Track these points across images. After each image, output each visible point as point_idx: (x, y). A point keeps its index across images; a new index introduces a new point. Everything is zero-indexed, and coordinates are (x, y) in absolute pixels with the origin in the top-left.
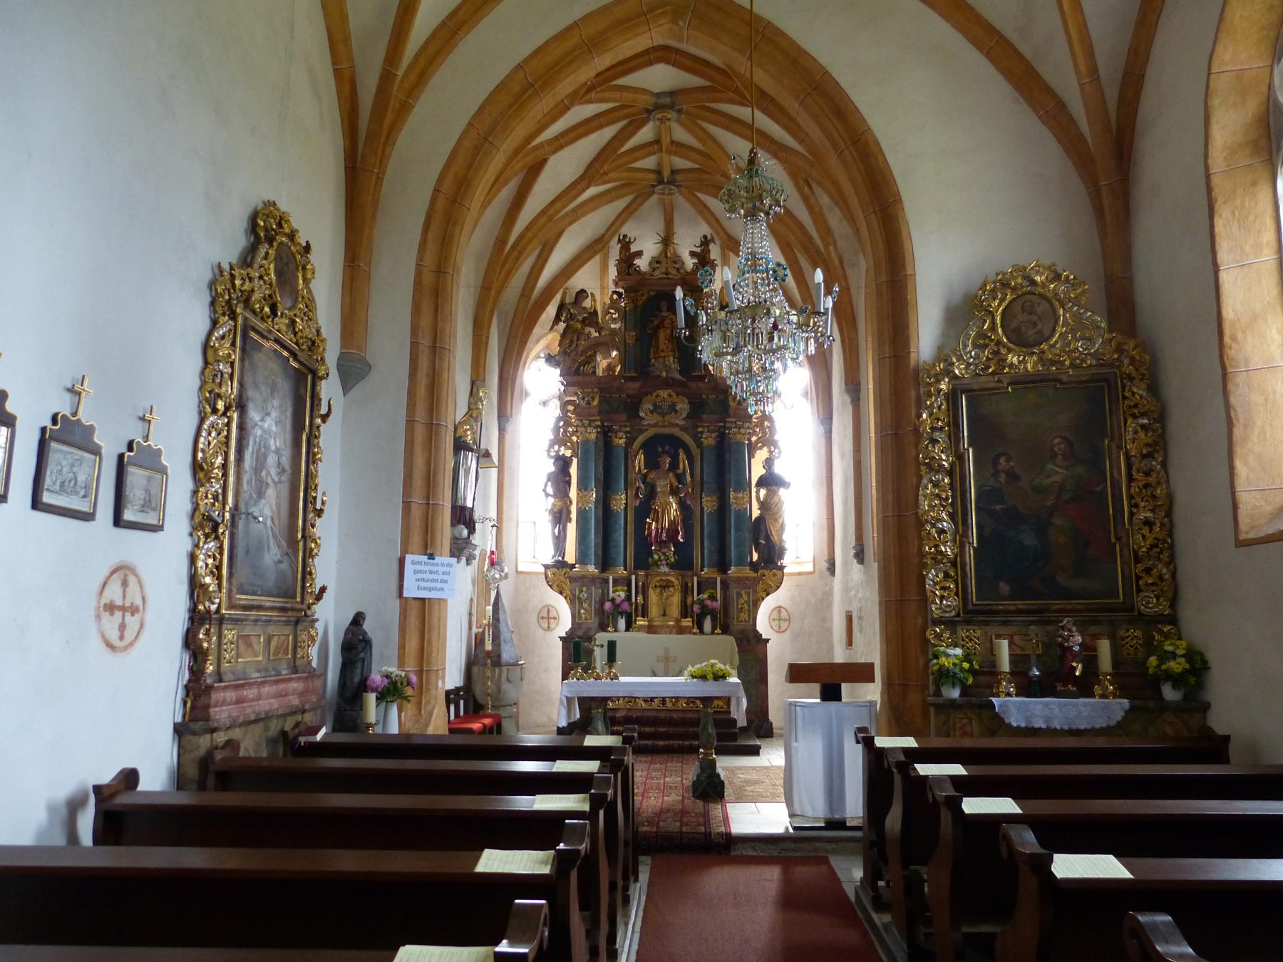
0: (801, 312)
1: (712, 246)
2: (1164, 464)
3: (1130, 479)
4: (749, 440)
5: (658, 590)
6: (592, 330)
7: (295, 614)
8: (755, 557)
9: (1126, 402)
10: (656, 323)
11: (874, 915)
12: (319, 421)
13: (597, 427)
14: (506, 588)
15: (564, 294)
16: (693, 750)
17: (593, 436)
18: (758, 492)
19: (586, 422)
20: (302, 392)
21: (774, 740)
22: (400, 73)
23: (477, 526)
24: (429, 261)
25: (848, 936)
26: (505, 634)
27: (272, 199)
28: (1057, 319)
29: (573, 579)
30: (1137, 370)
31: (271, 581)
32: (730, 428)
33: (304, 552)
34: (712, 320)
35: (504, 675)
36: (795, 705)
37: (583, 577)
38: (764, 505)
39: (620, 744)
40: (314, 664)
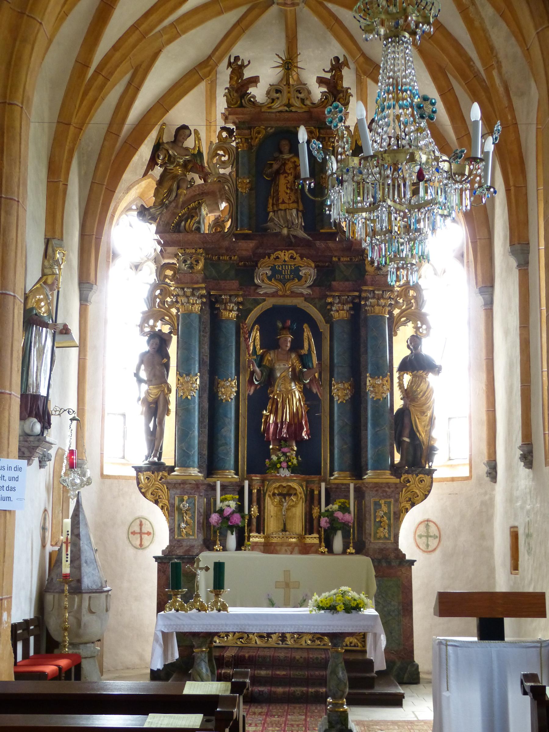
0: (454, 156)
1: (345, 72)
4: (390, 313)
6: (196, 176)
8: (397, 458)
10: (276, 167)
14: (88, 497)
15: (161, 131)
16: (320, 699)
17: (197, 308)
19: (188, 291)
21: (420, 686)
22: (206, 165)
23: (53, 418)
26: (86, 553)
29: (172, 486)
32: (366, 299)
34: (344, 168)
35: (85, 604)
36: (446, 644)
37: (184, 483)
38: (409, 395)
39: (228, 693)
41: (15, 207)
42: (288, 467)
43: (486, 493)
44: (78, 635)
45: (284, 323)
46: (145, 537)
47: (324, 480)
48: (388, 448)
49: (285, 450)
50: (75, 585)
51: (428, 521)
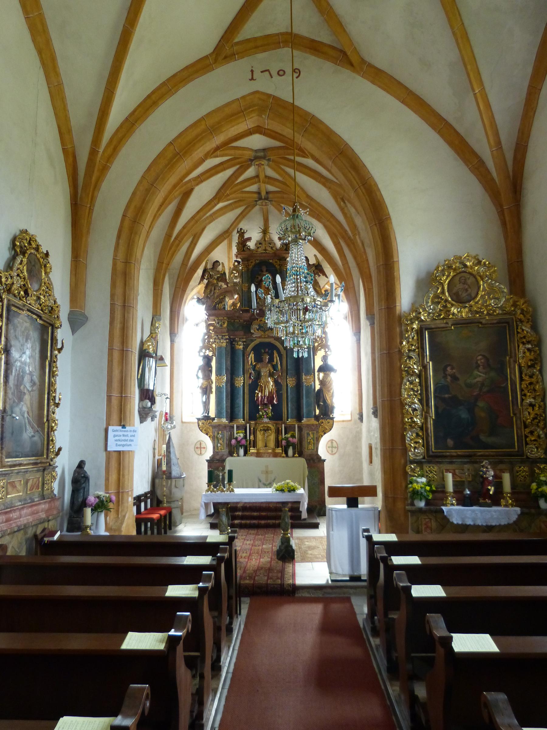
2: (541, 371)
3: (521, 380)
5: (262, 432)
6: (223, 284)
7: (42, 465)
8: (317, 412)
9: (519, 335)
11: (371, 639)
12: (56, 352)
13: (226, 339)
15: (206, 263)
17: (224, 344)
18: (318, 375)
20: (45, 337)
22: (101, 150)
24: (121, 256)
25: (357, 652)
27: (25, 228)
28: (479, 287)
29: (214, 427)
30: (525, 316)
31: (27, 448)
33: (48, 429)
35: (173, 484)
37: (219, 425)
38: (322, 383)
40: (56, 492)
41: (132, 310)
42: (267, 417)
43: (358, 428)
44: (170, 498)
45: (265, 350)
46: (202, 449)
47: (284, 423)
48: (313, 408)
49: (266, 409)
50: (169, 475)
51: (332, 440)
